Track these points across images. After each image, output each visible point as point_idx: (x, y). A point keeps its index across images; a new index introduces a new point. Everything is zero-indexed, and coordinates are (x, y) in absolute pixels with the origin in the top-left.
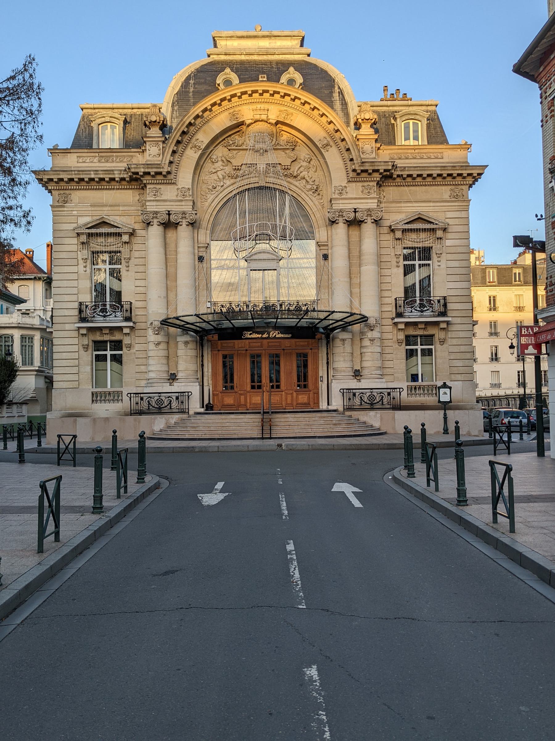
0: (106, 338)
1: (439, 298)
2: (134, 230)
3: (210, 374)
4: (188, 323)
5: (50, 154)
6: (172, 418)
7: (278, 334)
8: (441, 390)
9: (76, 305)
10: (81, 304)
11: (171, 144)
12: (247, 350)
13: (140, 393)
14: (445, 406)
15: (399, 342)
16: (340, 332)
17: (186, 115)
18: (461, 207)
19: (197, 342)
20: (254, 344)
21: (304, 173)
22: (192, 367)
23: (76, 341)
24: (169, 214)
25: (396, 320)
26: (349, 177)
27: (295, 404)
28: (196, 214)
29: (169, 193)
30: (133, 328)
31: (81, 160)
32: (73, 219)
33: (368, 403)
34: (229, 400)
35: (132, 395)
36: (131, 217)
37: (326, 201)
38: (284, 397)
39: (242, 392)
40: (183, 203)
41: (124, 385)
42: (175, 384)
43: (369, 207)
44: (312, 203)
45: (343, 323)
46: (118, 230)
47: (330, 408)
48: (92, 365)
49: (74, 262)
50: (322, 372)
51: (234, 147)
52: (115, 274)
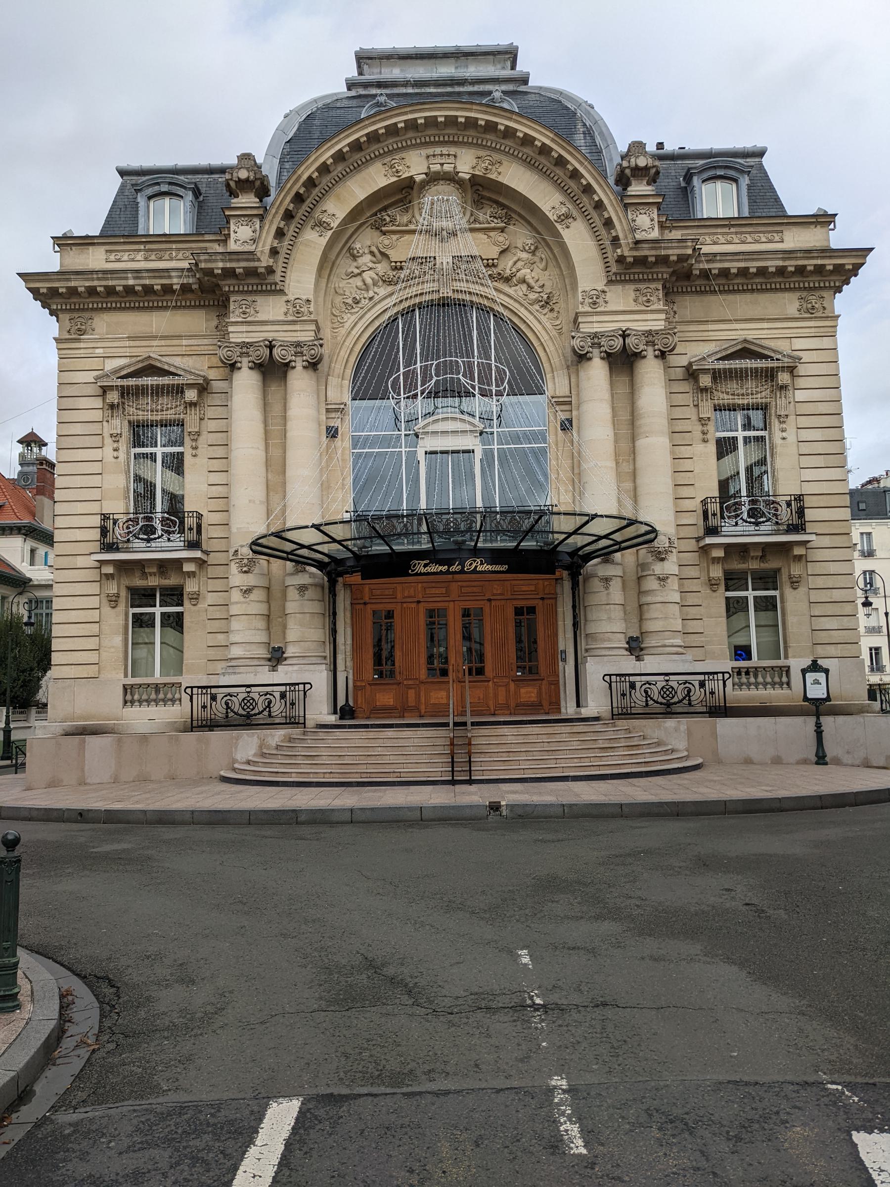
0: (153, 582)
1: (788, 498)
2: (207, 381)
3: (349, 648)
4: (302, 546)
5: (57, 248)
6: (273, 736)
7: (482, 564)
8: (808, 675)
9: (96, 521)
10: (105, 517)
11: (274, 217)
12: (419, 602)
13: (211, 687)
14: (817, 707)
15: (712, 584)
16: (600, 563)
17: (302, 164)
18: (822, 330)
19: (323, 587)
20: (433, 591)
21: (523, 271)
22: (316, 633)
23: (95, 588)
24: (271, 347)
25: (709, 540)
26: (610, 273)
27: (513, 704)
28: (321, 346)
29: (271, 309)
30: (205, 562)
31: (112, 257)
32: (95, 363)
33: (661, 704)
34: (386, 698)
35: (195, 690)
36: (202, 358)
37: (565, 321)
38: (491, 691)
39: (410, 682)
40: (297, 327)
41: (184, 670)
42: (280, 668)
43: (648, 328)
44: (542, 328)
45: (611, 542)
46: (176, 381)
47: (585, 712)
48: (126, 633)
49: (97, 441)
50: (565, 642)
51: (394, 228)
52: (176, 464)
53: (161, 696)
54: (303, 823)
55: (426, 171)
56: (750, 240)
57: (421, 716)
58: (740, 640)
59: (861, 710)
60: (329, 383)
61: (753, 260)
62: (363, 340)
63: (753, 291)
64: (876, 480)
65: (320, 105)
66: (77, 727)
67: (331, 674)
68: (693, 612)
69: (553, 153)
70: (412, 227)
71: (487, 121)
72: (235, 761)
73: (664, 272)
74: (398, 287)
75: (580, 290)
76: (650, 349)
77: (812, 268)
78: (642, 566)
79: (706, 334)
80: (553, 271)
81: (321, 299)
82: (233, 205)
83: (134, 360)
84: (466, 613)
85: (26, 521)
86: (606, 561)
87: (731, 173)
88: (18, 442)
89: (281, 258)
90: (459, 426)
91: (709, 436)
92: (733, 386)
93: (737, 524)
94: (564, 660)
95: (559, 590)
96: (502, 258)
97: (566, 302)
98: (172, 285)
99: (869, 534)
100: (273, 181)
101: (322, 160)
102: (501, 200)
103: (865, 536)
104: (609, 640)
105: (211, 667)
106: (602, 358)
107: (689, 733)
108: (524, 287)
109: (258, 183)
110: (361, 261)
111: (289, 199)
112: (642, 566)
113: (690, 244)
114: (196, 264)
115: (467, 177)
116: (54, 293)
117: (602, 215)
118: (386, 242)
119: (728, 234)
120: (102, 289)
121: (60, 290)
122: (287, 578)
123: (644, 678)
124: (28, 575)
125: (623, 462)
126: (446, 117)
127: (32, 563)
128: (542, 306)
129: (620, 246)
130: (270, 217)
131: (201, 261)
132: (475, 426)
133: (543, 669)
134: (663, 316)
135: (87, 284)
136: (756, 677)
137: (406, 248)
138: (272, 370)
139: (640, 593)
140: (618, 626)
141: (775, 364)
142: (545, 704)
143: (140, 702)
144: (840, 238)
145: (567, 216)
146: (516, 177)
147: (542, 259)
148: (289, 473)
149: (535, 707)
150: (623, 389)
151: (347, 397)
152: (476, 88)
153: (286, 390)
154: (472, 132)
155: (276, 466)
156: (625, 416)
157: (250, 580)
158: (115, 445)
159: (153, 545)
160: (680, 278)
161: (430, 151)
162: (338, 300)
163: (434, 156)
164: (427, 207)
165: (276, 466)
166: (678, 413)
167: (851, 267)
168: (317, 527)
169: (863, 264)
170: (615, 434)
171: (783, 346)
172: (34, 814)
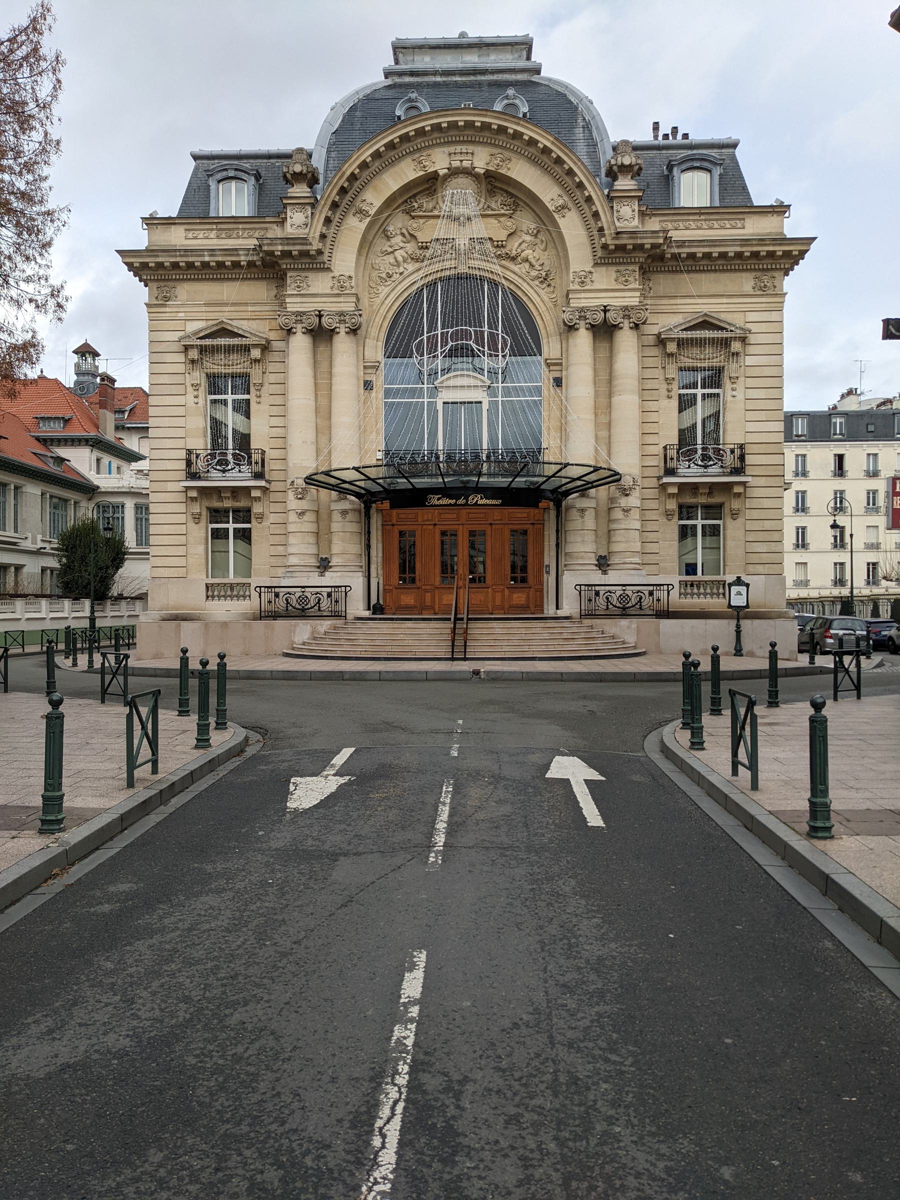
0: (228, 504)
1: (732, 446)
2: (268, 342)
3: (380, 560)
4: (345, 482)
5: (145, 226)
8: (732, 588)
9: (183, 454)
10: (189, 452)
12: (435, 525)
13: (275, 587)
14: (738, 613)
15: (668, 515)
16: (578, 497)
17: (346, 162)
19: (360, 512)
20: (447, 516)
21: (526, 252)
22: (356, 548)
23: (182, 508)
24: (320, 316)
25: (666, 480)
27: (506, 606)
28: (360, 315)
29: (320, 283)
30: (267, 489)
31: (190, 235)
32: (178, 325)
34: (408, 599)
35: (263, 589)
37: (559, 295)
38: (490, 595)
39: (428, 587)
40: (341, 299)
42: (327, 574)
44: (541, 302)
46: (244, 341)
47: (560, 613)
48: (207, 544)
49: (181, 390)
50: (549, 558)
51: (421, 213)
52: (244, 409)
53: (235, 593)
54: (347, 680)
55: (448, 166)
56: (716, 226)
57: (435, 614)
58: (689, 559)
59: (780, 616)
60: (366, 344)
61: (715, 246)
62: (394, 308)
63: (716, 271)
64: (890, 401)
65: (361, 96)
66: (171, 615)
67: (366, 579)
68: (652, 536)
69: (553, 154)
70: (436, 213)
71: (499, 125)
72: (293, 643)
73: (641, 257)
74: (425, 263)
75: (571, 270)
76: (626, 322)
77: (765, 254)
78: (612, 500)
79: (675, 307)
80: (551, 252)
81: (361, 274)
82: (289, 195)
83: (211, 323)
84: (472, 533)
85: (93, 434)
86: (583, 496)
87: (706, 164)
88: (74, 352)
89: (328, 241)
90: (472, 382)
91: (673, 393)
92: (695, 351)
93: (689, 467)
94: (548, 573)
95: (546, 517)
96: (510, 239)
97: (561, 278)
98: (240, 261)
99: (876, 455)
100: (321, 170)
101: (362, 158)
102: (510, 190)
103: (871, 457)
104: (582, 558)
105: (274, 572)
106: (587, 329)
107: (638, 630)
108: (527, 265)
109: (310, 175)
110: (393, 241)
111: (335, 192)
112: (612, 500)
113: (661, 235)
114: (260, 246)
115: (482, 171)
116: (145, 266)
117: (590, 209)
118: (415, 225)
119: (698, 220)
120: (184, 264)
121: (150, 265)
122: (332, 504)
123: (607, 588)
124: (96, 483)
125: (600, 416)
126: (465, 121)
127: (98, 473)
128: (541, 282)
129: (604, 236)
130: (320, 208)
131: (264, 245)
132: (484, 382)
133: (530, 578)
134: (638, 294)
135: (172, 260)
136: (699, 589)
137: (430, 231)
138: (321, 335)
139: (610, 521)
140: (590, 547)
141: (729, 335)
142: (532, 606)
143: (219, 597)
144: (792, 227)
145: (563, 207)
146: (522, 172)
147: (542, 241)
148: (334, 419)
149: (524, 608)
150: (603, 354)
151: (380, 357)
152: (495, 77)
153: (331, 350)
154: (487, 134)
155: (324, 414)
156: (603, 376)
157: (304, 505)
158: (196, 393)
159: (228, 475)
160: (654, 261)
161: (452, 149)
162: (375, 274)
163: (455, 153)
164: (448, 198)
165: (324, 414)
166: (648, 373)
167: (797, 253)
168: (356, 469)
169: (807, 251)
170: (596, 391)
171: (738, 320)
172: (158, 672)
